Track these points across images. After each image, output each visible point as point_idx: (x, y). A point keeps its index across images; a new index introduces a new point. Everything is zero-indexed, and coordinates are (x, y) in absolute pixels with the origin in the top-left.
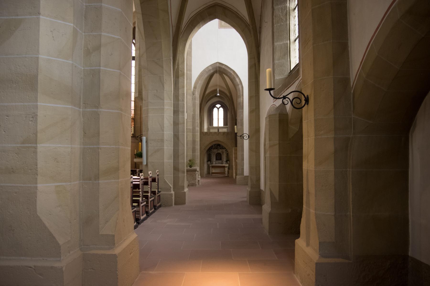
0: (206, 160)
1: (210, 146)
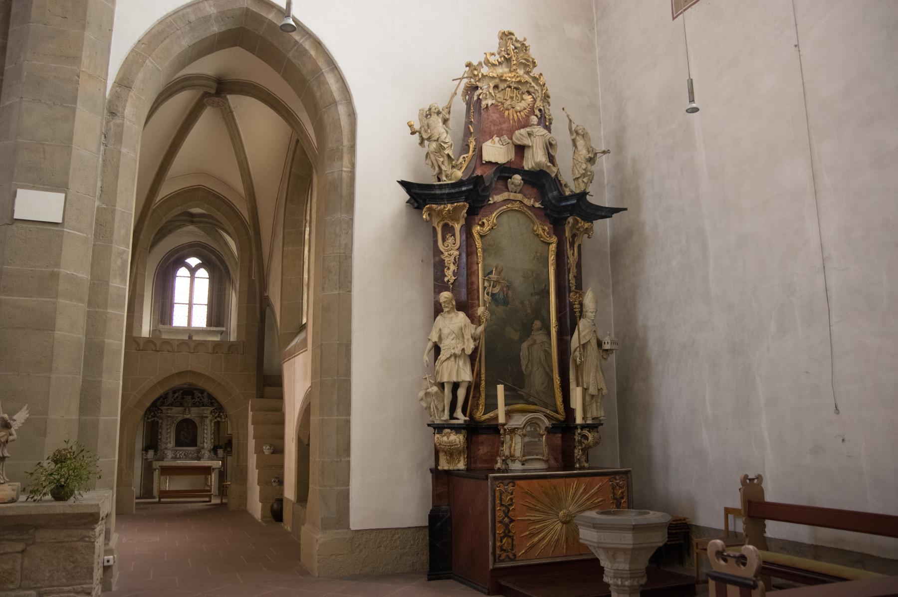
0: (139, 445)
1: (161, 391)
